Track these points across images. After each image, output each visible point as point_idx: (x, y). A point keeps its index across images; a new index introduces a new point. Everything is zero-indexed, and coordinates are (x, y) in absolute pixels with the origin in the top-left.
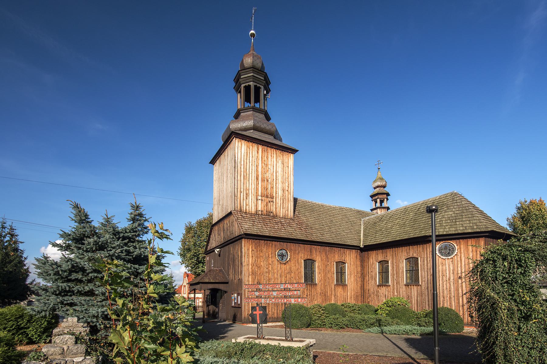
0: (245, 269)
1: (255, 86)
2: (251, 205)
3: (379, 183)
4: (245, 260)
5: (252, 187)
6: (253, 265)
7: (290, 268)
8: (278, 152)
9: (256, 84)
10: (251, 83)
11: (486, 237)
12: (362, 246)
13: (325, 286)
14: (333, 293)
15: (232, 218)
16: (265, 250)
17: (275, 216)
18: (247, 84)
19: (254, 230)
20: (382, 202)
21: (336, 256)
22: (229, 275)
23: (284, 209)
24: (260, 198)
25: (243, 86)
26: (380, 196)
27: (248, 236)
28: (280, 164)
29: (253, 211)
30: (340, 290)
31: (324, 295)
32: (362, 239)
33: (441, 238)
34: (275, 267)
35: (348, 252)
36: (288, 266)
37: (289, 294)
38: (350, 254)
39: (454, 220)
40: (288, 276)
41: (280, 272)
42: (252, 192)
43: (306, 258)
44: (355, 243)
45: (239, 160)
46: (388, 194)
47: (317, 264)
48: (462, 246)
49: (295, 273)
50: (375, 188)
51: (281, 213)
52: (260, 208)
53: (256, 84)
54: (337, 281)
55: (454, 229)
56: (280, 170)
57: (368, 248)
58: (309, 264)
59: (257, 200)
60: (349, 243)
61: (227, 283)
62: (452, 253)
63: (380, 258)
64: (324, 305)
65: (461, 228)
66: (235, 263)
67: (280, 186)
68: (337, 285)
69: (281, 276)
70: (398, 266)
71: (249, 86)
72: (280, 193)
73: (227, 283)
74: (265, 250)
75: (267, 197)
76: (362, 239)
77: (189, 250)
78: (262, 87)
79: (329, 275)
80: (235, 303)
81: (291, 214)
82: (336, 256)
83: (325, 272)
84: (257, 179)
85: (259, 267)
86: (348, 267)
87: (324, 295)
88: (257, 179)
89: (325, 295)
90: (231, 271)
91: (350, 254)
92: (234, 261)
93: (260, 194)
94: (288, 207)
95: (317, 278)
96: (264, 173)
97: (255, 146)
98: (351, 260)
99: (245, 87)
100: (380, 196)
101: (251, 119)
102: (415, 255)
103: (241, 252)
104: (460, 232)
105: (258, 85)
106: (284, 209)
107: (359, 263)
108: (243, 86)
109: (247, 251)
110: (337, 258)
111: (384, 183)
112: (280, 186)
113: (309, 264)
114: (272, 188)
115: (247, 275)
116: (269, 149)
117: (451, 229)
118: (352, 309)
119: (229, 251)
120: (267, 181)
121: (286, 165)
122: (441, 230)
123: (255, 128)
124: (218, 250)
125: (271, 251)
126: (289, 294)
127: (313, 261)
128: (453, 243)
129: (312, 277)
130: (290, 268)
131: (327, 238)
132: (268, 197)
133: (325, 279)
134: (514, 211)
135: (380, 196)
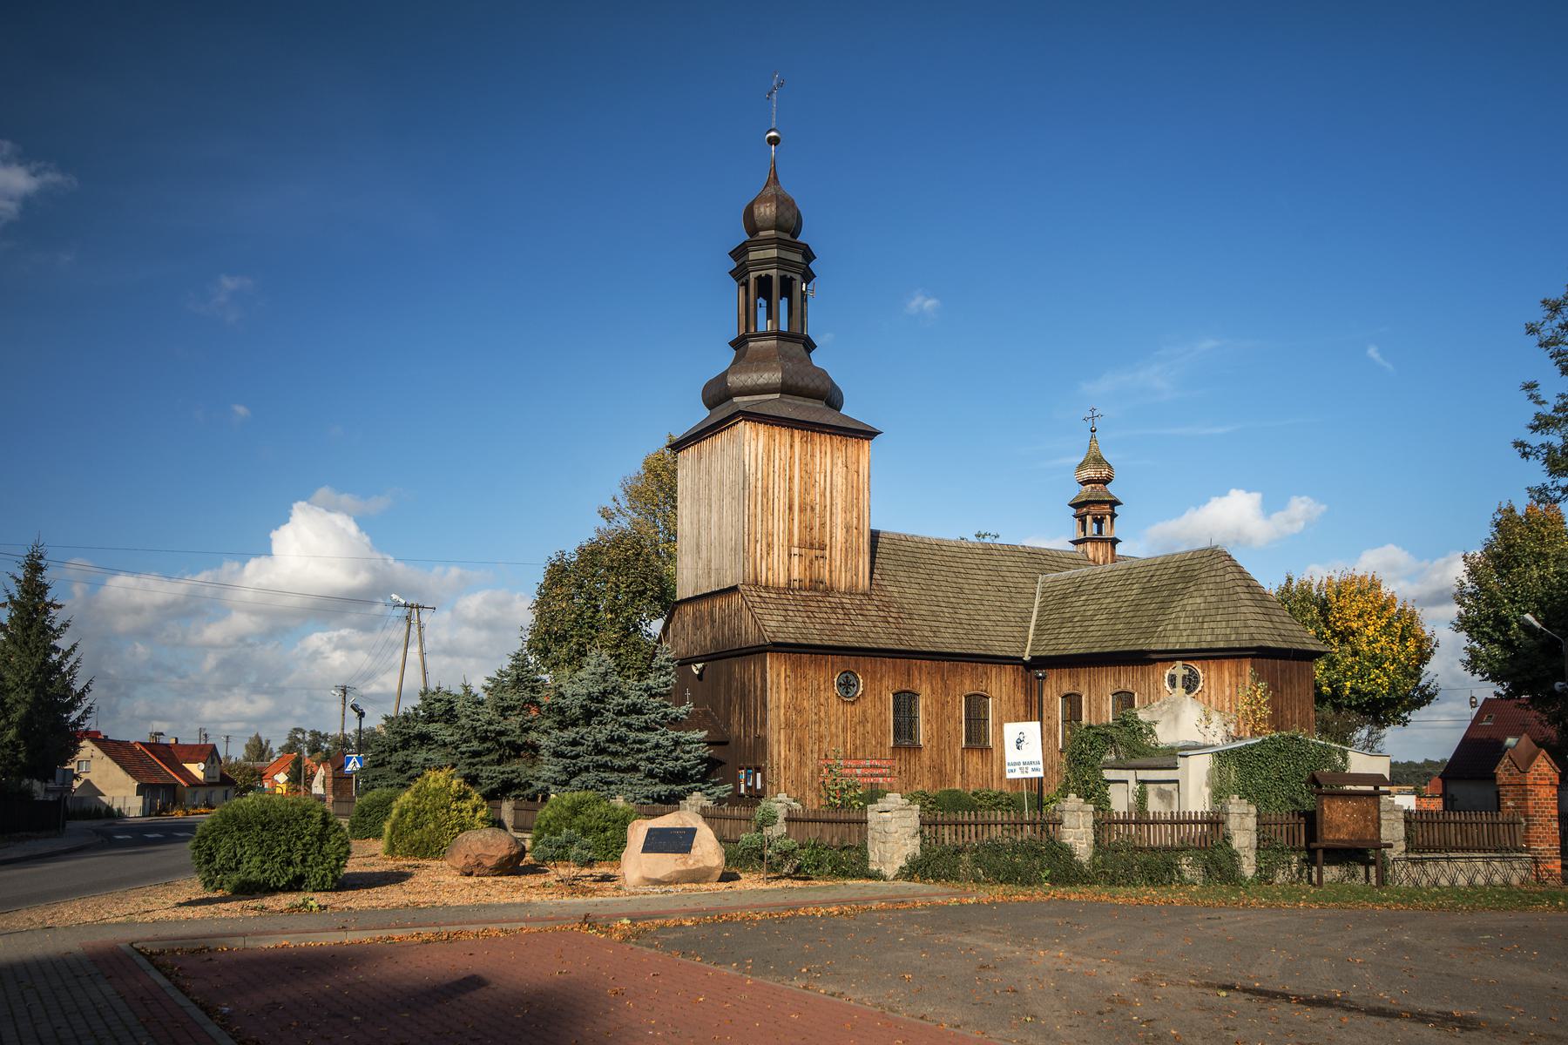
0: (771, 716)
1: (783, 278)
2: (780, 567)
3: (1090, 473)
4: (772, 698)
5: (779, 526)
6: (787, 708)
7: (864, 712)
8: (836, 439)
9: (783, 273)
10: (773, 272)
11: (1253, 657)
12: (1027, 658)
13: (940, 751)
14: (959, 766)
15: (736, 600)
16: (811, 673)
17: (829, 590)
18: (763, 273)
19: (789, 635)
20: (1099, 522)
21: (967, 682)
22: (728, 724)
23: (846, 569)
24: (796, 550)
25: (753, 275)
26: (1094, 509)
27: (779, 648)
28: (840, 469)
29: (782, 581)
30: (974, 760)
31: (938, 771)
32: (1031, 637)
33: (1169, 656)
34: (832, 711)
35: (994, 670)
36: (858, 708)
37: (877, 772)
38: (999, 675)
39: (1200, 619)
40: (860, 729)
41: (842, 721)
42: (779, 540)
43: (897, 689)
44: (1010, 651)
45: (753, 470)
46: (1114, 503)
47: (922, 702)
48: (1212, 674)
49: (873, 722)
50: (1084, 483)
51: (842, 581)
52: (795, 575)
53: (783, 273)
54: (968, 739)
55: (1195, 639)
56: (839, 481)
57: (1039, 663)
58: (905, 703)
59: (790, 555)
60: (998, 649)
61: (726, 743)
62: (1195, 687)
63: (1067, 688)
64: (936, 792)
65: (1209, 638)
66: (753, 704)
67: (839, 519)
68: (967, 748)
69: (844, 730)
70: (1099, 709)
71: (769, 278)
72: (840, 534)
73: (726, 743)
74: (811, 673)
75: (812, 546)
76: (1031, 637)
77: (561, 638)
78: (798, 277)
79: (950, 727)
80: (747, 788)
81: (863, 582)
82: (967, 682)
83: (941, 717)
84: (791, 508)
85: (799, 712)
86: (995, 707)
87: (938, 771)
88: (791, 508)
89: (940, 772)
90: (735, 719)
91: (999, 675)
92: (744, 696)
93: (796, 542)
94: (857, 567)
95: (923, 732)
96: (805, 490)
97: (786, 433)
98: (1000, 687)
99: (759, 278)
100: (1095, 508)
101: (775, 370)
102: (1129, 688)
103: (764, 680)
104: (1204, 646)
105: (789, 275)
106: (846, 569)
107: (1020, 696)
108: (753, 275)
109: (777, 675)
110: (968, 688)
111: (1104, 473)
112: (839, 519)
113: (905, 703)
114: (823, 525)
115: (776, 728)
116: (816, 436)
117: (1192, 639)
118: (994, 801)
119: (730, 675)
120: (813, 509)
121: (853, 467)
122: (1173, 640)
123: (786, 389)
124: (700, 665)
125: (823, 680)
126: (877, 772)
127: (913, 695)
128: (1197, 667)
129: (910, 710)
130: (864, 712)
131: (948, 641)
132: (814, 546)
133: (939, 735)
134: (1486, 532)
135: (1095, 508)
